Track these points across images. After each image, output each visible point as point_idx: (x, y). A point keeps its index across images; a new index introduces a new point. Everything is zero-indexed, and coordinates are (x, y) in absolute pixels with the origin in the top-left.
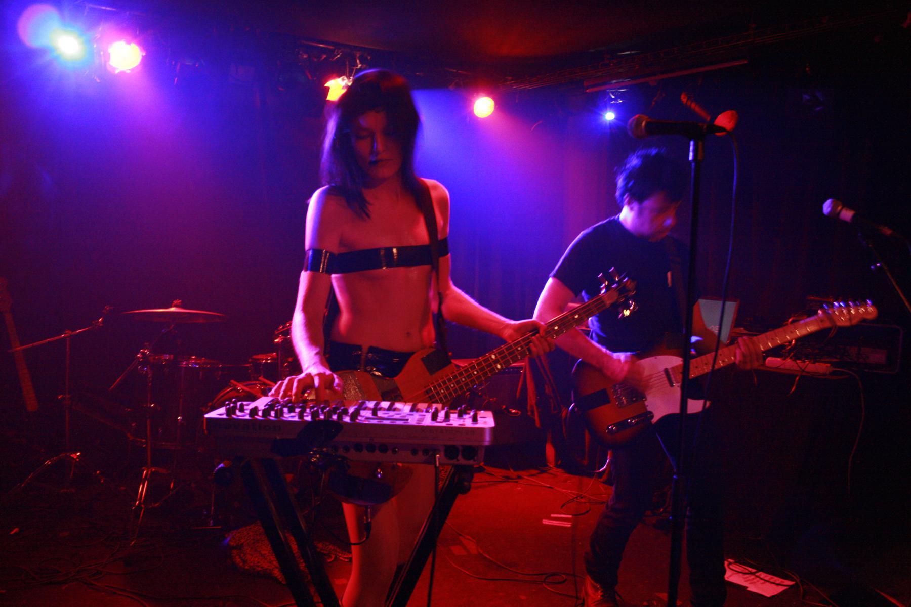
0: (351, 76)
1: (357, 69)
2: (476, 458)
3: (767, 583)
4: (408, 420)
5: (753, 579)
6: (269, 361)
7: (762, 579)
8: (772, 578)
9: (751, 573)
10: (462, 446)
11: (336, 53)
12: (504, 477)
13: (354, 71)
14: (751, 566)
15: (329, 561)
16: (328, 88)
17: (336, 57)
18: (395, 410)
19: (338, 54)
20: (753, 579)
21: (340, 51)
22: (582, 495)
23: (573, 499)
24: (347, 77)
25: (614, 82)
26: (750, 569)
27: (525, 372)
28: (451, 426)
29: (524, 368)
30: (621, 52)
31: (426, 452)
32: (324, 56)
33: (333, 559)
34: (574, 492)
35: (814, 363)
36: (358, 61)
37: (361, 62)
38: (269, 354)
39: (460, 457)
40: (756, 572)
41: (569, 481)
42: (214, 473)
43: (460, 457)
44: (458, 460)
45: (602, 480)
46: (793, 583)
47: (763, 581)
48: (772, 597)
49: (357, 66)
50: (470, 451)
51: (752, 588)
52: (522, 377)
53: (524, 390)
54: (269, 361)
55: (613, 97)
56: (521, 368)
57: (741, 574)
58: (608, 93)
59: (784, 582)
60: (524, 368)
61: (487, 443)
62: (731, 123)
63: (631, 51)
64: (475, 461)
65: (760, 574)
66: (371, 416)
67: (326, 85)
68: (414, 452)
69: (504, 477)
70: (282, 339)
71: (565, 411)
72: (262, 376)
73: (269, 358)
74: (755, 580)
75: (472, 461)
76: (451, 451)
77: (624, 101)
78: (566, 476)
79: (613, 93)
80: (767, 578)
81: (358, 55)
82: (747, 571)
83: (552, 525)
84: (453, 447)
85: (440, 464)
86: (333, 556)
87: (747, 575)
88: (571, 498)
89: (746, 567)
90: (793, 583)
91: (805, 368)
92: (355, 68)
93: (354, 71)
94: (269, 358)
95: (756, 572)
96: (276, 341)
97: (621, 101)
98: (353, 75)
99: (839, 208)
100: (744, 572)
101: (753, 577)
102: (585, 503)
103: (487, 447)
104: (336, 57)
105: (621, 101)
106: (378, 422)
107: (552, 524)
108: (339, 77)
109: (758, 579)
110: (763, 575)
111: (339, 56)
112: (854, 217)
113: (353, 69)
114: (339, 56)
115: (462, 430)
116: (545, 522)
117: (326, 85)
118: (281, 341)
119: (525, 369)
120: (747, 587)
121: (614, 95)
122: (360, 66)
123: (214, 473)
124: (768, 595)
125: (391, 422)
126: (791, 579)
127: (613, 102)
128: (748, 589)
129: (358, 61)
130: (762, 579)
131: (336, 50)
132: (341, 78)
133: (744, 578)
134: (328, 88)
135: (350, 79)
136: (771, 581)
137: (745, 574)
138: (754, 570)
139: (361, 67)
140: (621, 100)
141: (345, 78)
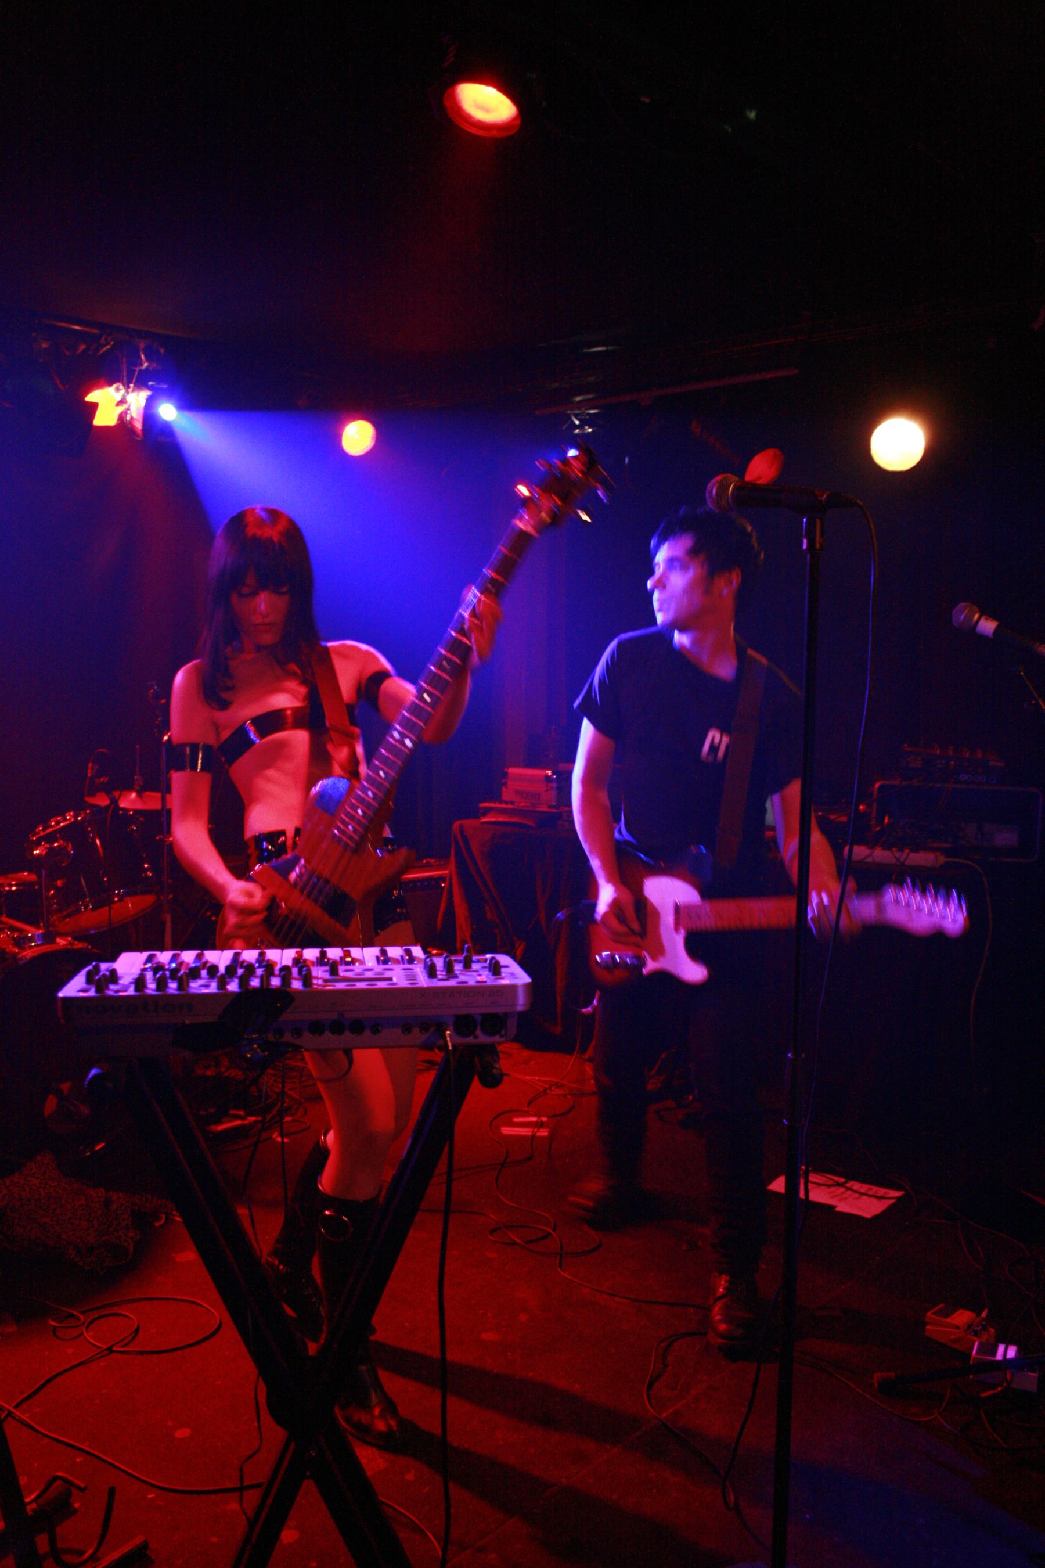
0: (131, 383)
1: (140, 371)
2: (503, 1032)
3: (865, 1198)
4: (391, 979)
5: (843, 1193)
6: (14, 888)
7: (856, 1192)
8: (870, 1189)
9: (838, 1184)
10: (482, 1015)
11: (103, 341)
12: (424, 1062)
13: (137, 373)
14: (836, 1173)
15: (157, 1224)
16: (94, 406)
17: (104, 349)
18: (353, 961)
19: (108, 344)
20: (843, 1193)
21: (110, 339)
22: (558, 1083)
23: (545, 1091)
24: (124, 385)
25: (578, 399)
26: (836, 1178)
27: (451, 885)
28: (465, 985)
29: (448, 879)
30: (589, 348)
31: (424, 1027)
32: (83, 347)
33: (163, 1221)
34: (544, 1079)
35: (917, 851)
36: (143, 357)
37: (148, 359)
38: (10, 876)
39: (478, 1032)
40: (845, 1182)
41: (533, 1062)
42: (86, 1083)
43: (478, 1032)
44: (476, 1037)
45: (587, 1056)
46: (903, 1193)
47: (857, 1195)
48: (876, 1218)
49: (142, 365)
50: (494, 1022)
51: (842, 1207)
52: (445, 894)
53: (450, 916)
54: (14, 888)
55: (577, 422)
56: (442, 879)
57: (824, 1188)
58: (569, 417)
59: (889, 1193)
60: (448, 879)
61: (520, 1008)
62: (773, 470)
63: (607, 346)
64: (502, 1036)
65: (853, 1185)
66: (327, 976)
67: (90, 398)
68: (407, 1029)
69: (424, 1062)
70: (46, 848)
71: (521, 947)
72: (4, 915)
73: (13, 883)
74: (845, 1196)
75: (472, 1037)
76: (464, 1024)
77: (595, 429)
78: (526, 1053)
79: (576, 416)
80: (862, 1191)
81: (142, 346)
82: (831, 1182)
83: (519, 1136)
84: (467, 1017)
85: (453, 1046)
86: (164, 1217)
87: (833, 1188)
88: (542, 1089)
89: (829, 1176)
90: (903, 1193)
91: (905, 859)
92: (138, 369)
93: (137, 373)
94: (13, 883)
95: (845, 1182)
96: (36, 852)
97: (590, 430)
98: (134, 380)
99: (976, 617)
100: (828, 1183)
101: (842, 1190)
102: (565, 1095)
103: (521, 1015)
104: (104, 349)
105: (590, 430)
106: (355, 985)
107: (518, 1133)
108: (110, 385)
109: (849, 1192)
110: (856, 1186)
111: (108, 347)
112: (996, 631)
113: (135, 371)
114: (108, 347)
115: (480, 990)
116: (506, 1131)
117: (90, 398)
118: (44, 852)
119: (451, 879)
120: (834, 1207)
121: (578, 420)
122: (146, 364)
123: (86, 1083)
124: (868, 1215)
125: (355, 985)
126: (898, 1188)
127: (577, 431)
128: (837, 1209)
129: (143, 357)
130: (856, 1192)
131: (104, 337)
132: (114, 386)
133: (829, 1193)
134: (94, 406)
135: (129, 387)
136: (870, 1193)
137: (829, 1186)
138: (842, 1180)
139: (149, 366)
140: (590, 428)
141: (121, 387)
